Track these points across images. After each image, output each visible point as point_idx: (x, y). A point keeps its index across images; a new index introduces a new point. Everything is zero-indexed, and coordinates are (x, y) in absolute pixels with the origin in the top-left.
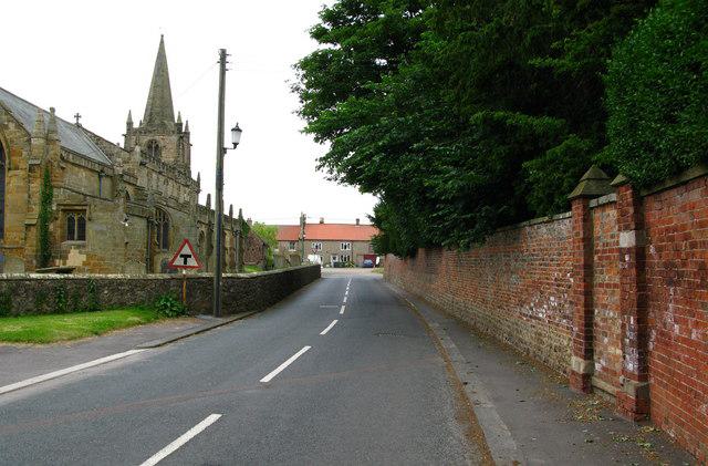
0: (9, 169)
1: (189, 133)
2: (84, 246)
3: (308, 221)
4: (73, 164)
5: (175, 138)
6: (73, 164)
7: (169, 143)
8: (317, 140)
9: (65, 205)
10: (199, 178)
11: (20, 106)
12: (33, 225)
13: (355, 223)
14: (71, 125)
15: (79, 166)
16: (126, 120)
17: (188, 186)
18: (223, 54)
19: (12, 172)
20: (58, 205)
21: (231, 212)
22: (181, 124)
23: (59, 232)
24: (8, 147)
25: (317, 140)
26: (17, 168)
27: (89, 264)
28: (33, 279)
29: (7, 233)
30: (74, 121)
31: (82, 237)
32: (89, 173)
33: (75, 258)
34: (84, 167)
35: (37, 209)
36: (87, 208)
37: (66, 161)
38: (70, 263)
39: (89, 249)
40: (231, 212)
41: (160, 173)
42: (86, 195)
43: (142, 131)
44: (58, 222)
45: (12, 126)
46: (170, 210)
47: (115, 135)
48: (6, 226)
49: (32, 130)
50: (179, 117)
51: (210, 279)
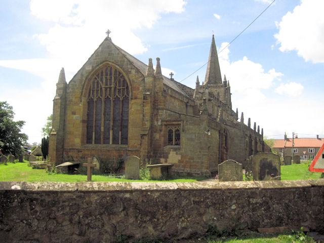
0: (132, 99)
1: (230, 87)
2: (179, 149)
4: (171, 96)
5: (223, 89)
6: (171, 96)
9: (166, 121)
10: (237, 112)
11: (139, 64)
12: (146, 135)
14: (168, 79)
15: (175, 98)
16: (196, 81)
19: (133, 101)
20: (162, 121)
22: (226, 81)
23: (162, 139)
26: (136, 98)
27: (183, 162)
30: (169, 77)
34: (178, 99)
39: (183, 151)
41: (219, 106)
42: (180, 114)
43: (206, 87)
44: (162, 133)
45: (133, 72)
46: (228, 128)
48: (129, 135)
50: (225, 78)
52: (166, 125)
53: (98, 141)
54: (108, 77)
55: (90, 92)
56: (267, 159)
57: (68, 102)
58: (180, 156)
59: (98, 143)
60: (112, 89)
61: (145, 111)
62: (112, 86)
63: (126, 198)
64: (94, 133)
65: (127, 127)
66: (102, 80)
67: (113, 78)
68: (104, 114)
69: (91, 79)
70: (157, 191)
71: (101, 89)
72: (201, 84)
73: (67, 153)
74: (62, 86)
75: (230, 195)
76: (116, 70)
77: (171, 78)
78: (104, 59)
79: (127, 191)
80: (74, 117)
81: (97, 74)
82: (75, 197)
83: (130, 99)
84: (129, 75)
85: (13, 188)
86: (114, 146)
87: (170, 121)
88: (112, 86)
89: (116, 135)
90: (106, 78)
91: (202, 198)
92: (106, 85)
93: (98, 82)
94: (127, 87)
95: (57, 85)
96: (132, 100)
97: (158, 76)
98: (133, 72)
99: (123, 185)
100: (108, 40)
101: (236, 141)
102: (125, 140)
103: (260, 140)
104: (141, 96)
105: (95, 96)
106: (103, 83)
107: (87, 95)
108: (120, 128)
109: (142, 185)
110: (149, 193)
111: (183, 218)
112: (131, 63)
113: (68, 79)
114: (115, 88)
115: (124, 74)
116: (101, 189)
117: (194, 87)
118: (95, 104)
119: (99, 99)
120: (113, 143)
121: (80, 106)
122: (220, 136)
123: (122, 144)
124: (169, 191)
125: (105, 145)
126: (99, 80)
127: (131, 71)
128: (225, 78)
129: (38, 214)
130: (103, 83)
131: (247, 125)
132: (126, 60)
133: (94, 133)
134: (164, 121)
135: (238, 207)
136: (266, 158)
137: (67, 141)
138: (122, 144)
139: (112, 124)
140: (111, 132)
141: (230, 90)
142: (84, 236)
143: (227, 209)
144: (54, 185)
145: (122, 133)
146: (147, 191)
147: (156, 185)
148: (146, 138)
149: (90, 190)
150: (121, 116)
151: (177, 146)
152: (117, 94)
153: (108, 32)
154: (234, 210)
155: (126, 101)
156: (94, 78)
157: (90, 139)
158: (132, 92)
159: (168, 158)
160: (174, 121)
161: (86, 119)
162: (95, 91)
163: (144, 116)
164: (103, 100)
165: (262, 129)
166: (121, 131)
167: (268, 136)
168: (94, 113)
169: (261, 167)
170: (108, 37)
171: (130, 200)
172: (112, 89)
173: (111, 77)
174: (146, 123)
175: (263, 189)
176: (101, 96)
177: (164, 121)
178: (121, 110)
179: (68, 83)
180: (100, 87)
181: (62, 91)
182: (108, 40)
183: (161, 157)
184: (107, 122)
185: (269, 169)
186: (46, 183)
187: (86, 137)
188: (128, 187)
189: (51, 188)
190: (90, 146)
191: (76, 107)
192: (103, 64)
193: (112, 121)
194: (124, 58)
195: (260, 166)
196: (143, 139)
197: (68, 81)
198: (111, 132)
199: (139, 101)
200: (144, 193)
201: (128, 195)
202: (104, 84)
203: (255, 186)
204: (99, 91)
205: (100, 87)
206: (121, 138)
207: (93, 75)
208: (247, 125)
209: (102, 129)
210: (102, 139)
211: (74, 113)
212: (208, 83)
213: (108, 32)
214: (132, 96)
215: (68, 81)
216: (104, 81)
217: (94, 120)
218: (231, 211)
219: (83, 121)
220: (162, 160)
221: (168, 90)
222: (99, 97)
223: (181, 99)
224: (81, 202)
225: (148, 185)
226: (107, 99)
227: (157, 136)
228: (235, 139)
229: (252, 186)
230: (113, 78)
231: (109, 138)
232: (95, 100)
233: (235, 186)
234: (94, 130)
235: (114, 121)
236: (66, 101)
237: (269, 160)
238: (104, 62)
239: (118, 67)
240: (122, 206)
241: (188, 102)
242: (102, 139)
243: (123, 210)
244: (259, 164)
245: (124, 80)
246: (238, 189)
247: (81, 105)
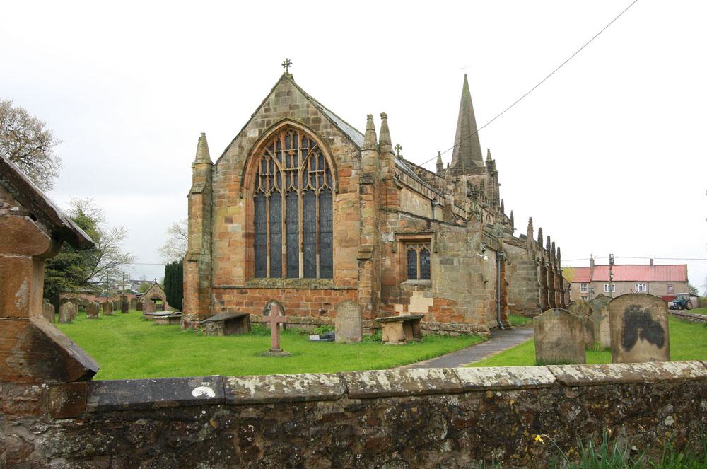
0: (337, 193)
2: (429, 286)
3: (616, 262)
8: (9, 104)
9: (404, 234)
13: (649, 263)
15: (413, 190)
20: (396, 234)
23: (398, 268)
24: (335, 166)
25: (9, 104)
26: (345, 191)
27: (437, 310)
29: (336, 272)
31: (426, 274)
34: (418, 192)
42: (429, 221)
44: (397, 256)
48: (335, 262)
49: (360, 142)
50: (489, 156)
52: (403, 241)
53: (275, 272)
54: (291, 151)
57: (216, 201)
58: (432, 299)
59: (276, 277)
60: (300, 174)
61: (364, 216)
63: (451, 407)
64: (268, 258)
65: (330, 245)
66: (279, 153)
67: (300, 153)
68: (286, 222)
69: (258, 156)
70: (514, 388)
71: (278, 172)
72: (445, 167)
73: (219, 296)
74: (204, 168)
75: (661, 394)
76: (304, 137)
78: (282, 118)
79: (453, 392)
80: (230, 227)
81: (269, 144)
82: (342, 410)
84: (331, 147)
85: (197, 393)
86: (306, 281)
89: (311, 260)
90: (286, 152)
91: (607, 401)
92: (288, 166)
93: (271, 160)
94: (328, 170)
95: (194, 166)
96: (338, 195)
97: (383, 148)
98: (338, 140)
99: (443, 377)
100: (287, 78)
102: (327, 270)
103: (556, 268)
105: (268, 188)
106: (281, 162)
108: (316, 248)
109: (483, 375)
110: (499, 394)
111: (572, 450)
112: (334, 124)
113: (215, 155)
114: (305, 171)
115: (321, 145)
116: (399, 388)
117: (433, 168)
118: (267, 202)
119: (275, 192)
120: (305, 276)
121: (240, 207)
122: (497, 261)
123: (321, 277)
124: (540, 387)
125: (290, 280)
126: (274, 156)
127: (333, 140)
128: (489, 156)
129: (261, 456)
130: (281, 162)
132: (323, 118)
133: (268, 258)
134: (399, 234)
135: (679, 421)
136: (636, 304)
137: (218, 272)
138: (321, 277)
139: (301, 240)
140: (301, 255)
143: (656, 424)
144: (291, 383)
145: (320, 258)
146: (494, 389)
147: (510, 374)
149: (375, 390)
150: (317, 225)
151: (424, 282)
152: (309, 183)
153: (287, 64)
154: (671, 428)
155: (326, 194)
156: (263, 152)
157: (261, 269)
158: (337, 179)
160: (419, 234)
163: (362, 224)
164: (282, 195)
166: (320, 253)
167: (572, 259)
168: (268, 220)
171: (462, 410)
172: (300, 174)
174: (367, 237)
176: (280, 187)
177: (399, 234)
178: (317, 215)
179: (214, 163)
182: (287, 78)
184: (292, 237)
185: (643, 327)
186: (272, 378)
187: (252, 264)
188: (454, 380)
189: (285, 389)
190: (263, 282)
191: (231, 210)
192: (274, 130)
193: (301, 236)
194: (320, 115)
195: (625, 321)
196: (364, 267)
198: (301, 255)
199: (352, 197)
200: (490, 394)
201: (454, 400)
202: (284, 164)
204: (275, 178)
206: (320, 266)
207: (261, 147)
209: (284, 250)
210: (284, 270)
211: (229, 220)
212: (459, 165)
213: (287, 64)
214: (337, 187)
217: (268, 232)
218: (664, 431)
219: (247, 236)
220: (399, 308)
224: (356, 420)
225: (492, 374)
226: (291, 192)
230: (300, 153)
233: (667, 372)
234: (268, 253)
235: (305, 233)
237: (643, 309)
238: (281, 121)
239: (309, 132)
240: (445, 427)
242: (284, 270)
245: (321, 156)
246: (675, 380)
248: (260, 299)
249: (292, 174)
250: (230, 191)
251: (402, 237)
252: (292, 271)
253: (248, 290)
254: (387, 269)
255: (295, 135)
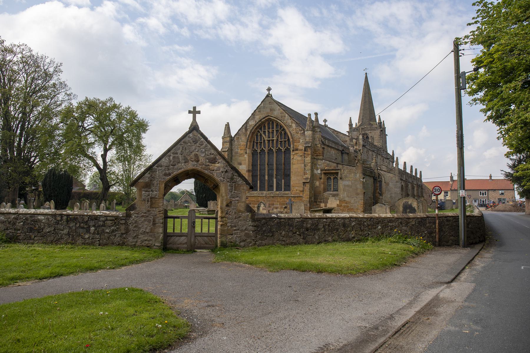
0: (293, 151)
2: (337, 195)
5: (378, 132)
7: (375, 135)
9: (326, 170)
13: (488, 178)
15: (331, 147)
17: (388, 159)
18: (350, 118)
20: (321, 170)
21: (411, 171)
22: (381, 123)
23: (322, 186)
24: (292, 138)
26: (297, 150)
27: (341, 206)
28: (329, 218)
29: (292, 188)
32: (336, 152)
33: (332, 203)
34: (334, 148)
35: (309, 172)
36: (339, 171)
37: (324, 144)
38: (329, 205)
40: (411, 171)
44: (322, 180)
46: (382, 172)
47: (344, 129)
48: (292, 183)
51: (456, 218)
52: (325, 173)
54: (271, 130)
55: (254, 145)
56: (408, 202)
62: (275, 138)
64: (258, 182)
66: (264, 132)
67: (275, 132)
68: (267, 164)
71: (264, 141)
72: (354, 126)
76: (277, 124)
77: (325, 124)
81: (260, 127)
83: (291, 151)
86: (278, 192)
87: (329, 170)
88: (275, 138)
90: (268, 131)
92: (269, 137)
93: (261, 135)
94: (289, 140)
100: (269, 96)
101: (391, 185)
102: (288, 187)
104: (301, 147)
106: (265, 135)
107: (251, 147)
114: (277, 140)
115: (285, 128)
120: (277, 190)
126: (262, 133)
127: (291, 125)
130: (265, 135)
131: (402, 169)
133: (258, 182)
141: (385, 131)
142: (305, 239)
148: (308, 186)
151: (335, 192)
153: (269, 89)
156: (257, 131)
158: (293, 145)
159: (327, 202)
160: (333, 170)
161: (251, 168)
162: (259, 144)
163: (305, 165)
165: (421, 172)
169: (404, 208)
170: (269, 94)
173: (273, 131)
175: (397, 218)
176: (265, 148)
179: (233, 136)
180: (263, 140)
181: (228, 144)
182: (269, 96)
183: (321, 202)
184: (270, 171)
197: (233, 134)
198: (275, 180)
199: (300, 153)
203: (391, 216)
204: (262, 144)
205: (263, 140)
207: (256, 129)
208: (402, 169)
214: (293, 148)
215: (233, 134)
216: (267, 134)
221: (325, 141)
222: (262, 149)
223: (336, 148)
227: (317, 183)
228: (390, 183)
229: (389, 216)
230: (275, 132)
231: (272, 186)
232: (259, 151)
236: (232, 153)
237: (409, 203)
241: (343, 150)
242: (266, 187)
243: (323, 227)
244: (402, 205)
247: (246, 156)
248: (254, 201)
249: (271, 142)
250: (240, 150)
251: (324, 172)
252: (270, 188)
253: (249, 197)
254: (317, 187)
255: (273, 123)
